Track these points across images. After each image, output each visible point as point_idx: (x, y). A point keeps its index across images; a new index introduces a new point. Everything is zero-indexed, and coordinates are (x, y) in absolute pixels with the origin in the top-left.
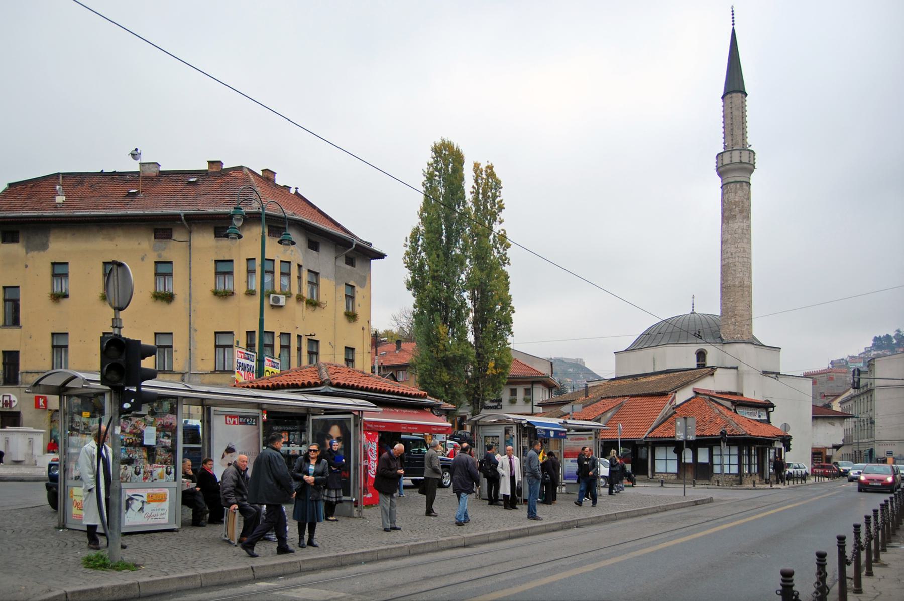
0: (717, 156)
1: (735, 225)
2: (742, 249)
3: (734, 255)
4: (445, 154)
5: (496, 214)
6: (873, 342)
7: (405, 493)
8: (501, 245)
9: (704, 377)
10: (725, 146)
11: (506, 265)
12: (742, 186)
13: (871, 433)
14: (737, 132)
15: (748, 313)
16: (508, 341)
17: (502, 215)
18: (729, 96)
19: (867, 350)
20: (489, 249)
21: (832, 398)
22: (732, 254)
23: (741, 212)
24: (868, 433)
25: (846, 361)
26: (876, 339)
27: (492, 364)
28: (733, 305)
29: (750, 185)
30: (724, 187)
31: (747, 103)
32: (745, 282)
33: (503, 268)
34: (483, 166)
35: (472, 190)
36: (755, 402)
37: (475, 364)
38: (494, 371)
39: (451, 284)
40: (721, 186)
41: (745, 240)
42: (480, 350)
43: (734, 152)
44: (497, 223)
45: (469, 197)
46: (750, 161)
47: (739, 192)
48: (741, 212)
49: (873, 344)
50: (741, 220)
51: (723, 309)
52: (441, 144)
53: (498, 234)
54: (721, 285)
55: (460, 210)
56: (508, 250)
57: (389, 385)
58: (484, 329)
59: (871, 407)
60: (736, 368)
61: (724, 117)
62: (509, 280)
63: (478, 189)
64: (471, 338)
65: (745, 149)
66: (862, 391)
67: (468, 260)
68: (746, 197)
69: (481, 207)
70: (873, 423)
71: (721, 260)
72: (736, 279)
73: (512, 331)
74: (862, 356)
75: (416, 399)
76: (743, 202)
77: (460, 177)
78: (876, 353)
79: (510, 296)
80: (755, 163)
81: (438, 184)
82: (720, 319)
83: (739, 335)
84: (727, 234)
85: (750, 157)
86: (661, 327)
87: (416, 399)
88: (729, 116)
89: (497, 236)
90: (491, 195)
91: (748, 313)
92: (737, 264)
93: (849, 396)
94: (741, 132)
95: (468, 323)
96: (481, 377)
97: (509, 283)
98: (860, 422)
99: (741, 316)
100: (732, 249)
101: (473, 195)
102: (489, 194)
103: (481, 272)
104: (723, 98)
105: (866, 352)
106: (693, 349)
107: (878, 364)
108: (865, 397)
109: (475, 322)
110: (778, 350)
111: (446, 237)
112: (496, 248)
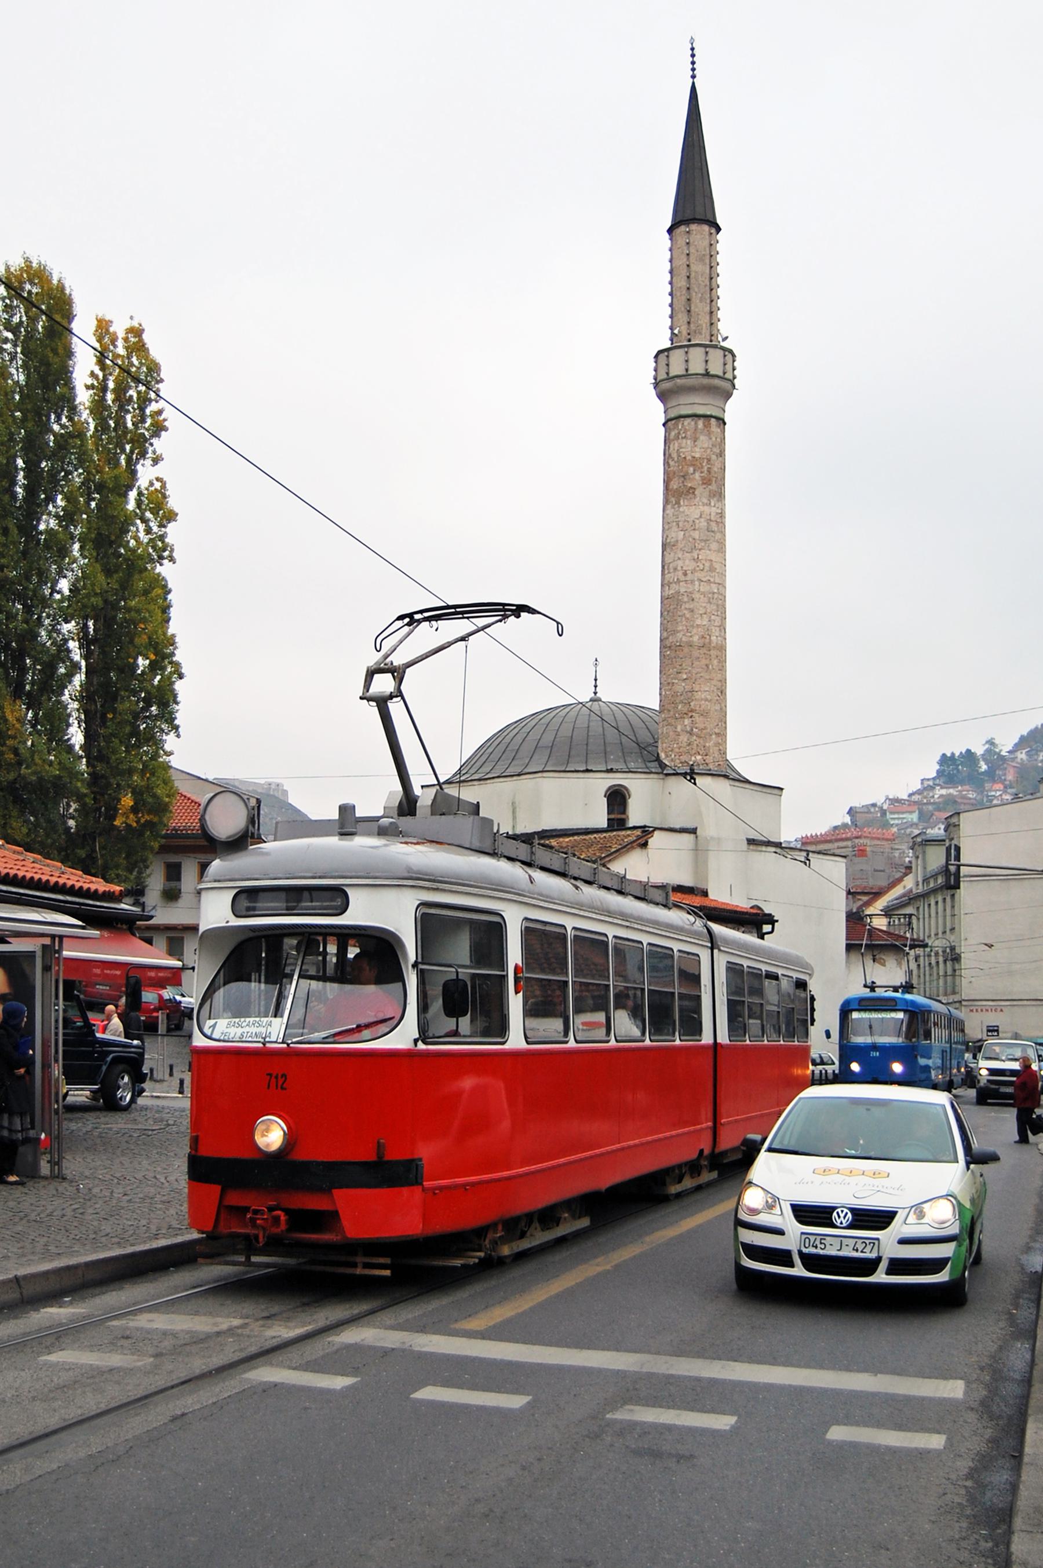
0: (656, 357)
1: (693, 510)
2: (707, 564)
3: (689, 577)
4: (30, 292)
5: (146, 440)
6: (938, 767)
7: (74, 1126)
8: (155, 513)
9: (628, 851)
10: (673, 333)
11: (165, 562)
12: (707, 426)
13: (954, 983)
14: (700, 308)
15: (718, 707)
16: (167, 747)
17: (159, 445)
18: (683, 228)
19: (926, 783)
20: (125, 524)
21: (865, 898)
22: (685, 574)
23: (706, 482)
24: (946, 983)
25: (881, 808)
26: (946, 760)
27: (127, 801)
28: (688, 688)
29: (725, 424)
30: (669, 423)
31: (719, 247)
32: (713, 638)
33: (159, 569)
34: (119, 329)
35: (89, 381)
36: (736, 912)
37: (87, 800)
38: (132, 820)
39: (35, 602)
40: (663, 421)
41: (714, 546)
42: (100, 767)
43: (691, 349)
44: (148, 462)
45: (83, 397)
46: (724, 373)
47: (702, 438)
48: (706, 482)
49: (938, 772)
50: (705, 501)
51: (666, 696)
52: (21, 269)
53: (147, 489)
54: (661, 641)
55: (63, 426)
56: (171, 528)
57: (47, 870)
58: (110, 716)
59: (953, 923)
60: (693, 831)
61: (671, 272)
62: (170, 597)
63: (105, 379)
64: (76, 736)
65: (715, 347)
66: (932, 885)
67: (77, 546)
68: (717, 450)
69: (112, 423)
70: (956, 959)
71: (662, 586)
72: (695, 631)
73: (177, 722)
74: (916, 798)
75: (105, 905)
76: (709, 460)
77: (65, 349)
78: (944, 792)
79: (173, 636)
80: (734, 377)
81: (11, 360)
82: (656, 719)
83: (699, 757)
84: (675, 528)
85: (725, 364)
86: (527, 729)
87: (105, 905)
88: (684, 272)
89: (146, 492)
90: (135, 395)
91: (718, 707)
92: (696, 596)
93: (904, 895)
94: (708, 308)
95: (70, 697)
96: (100, 834)
97: (169, 606)
98: (929, 956)
99: (705, 714)
100: (687, 562)
101: (91, 392)
102: (132, 392)
103: (106, 577)
104: (670, 231)
105: (925, 789)
106: (602, 783)
107: (968, 823)
108: (940, 899)
109: (86, 697)
110: (776, 791)
111: (26, 488)
112: (144, 521)
